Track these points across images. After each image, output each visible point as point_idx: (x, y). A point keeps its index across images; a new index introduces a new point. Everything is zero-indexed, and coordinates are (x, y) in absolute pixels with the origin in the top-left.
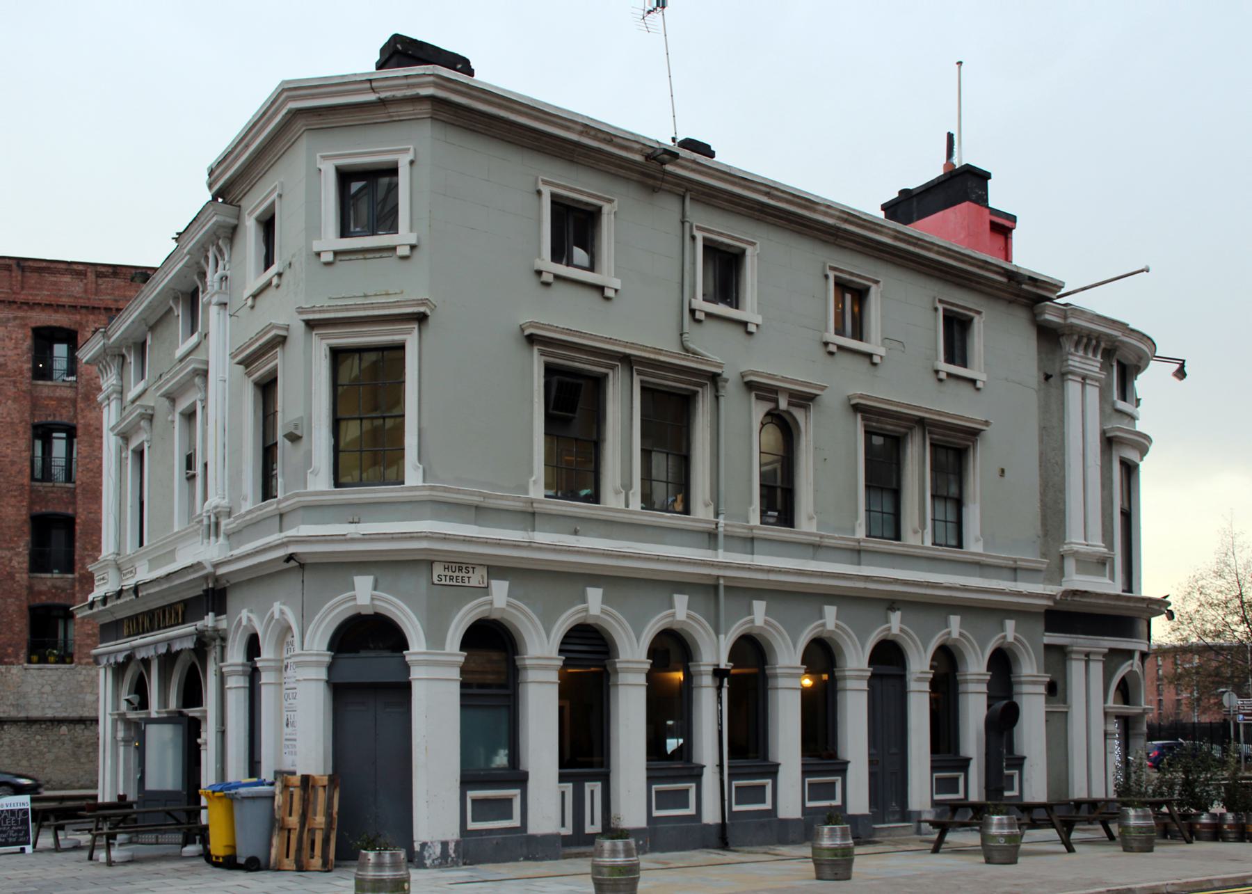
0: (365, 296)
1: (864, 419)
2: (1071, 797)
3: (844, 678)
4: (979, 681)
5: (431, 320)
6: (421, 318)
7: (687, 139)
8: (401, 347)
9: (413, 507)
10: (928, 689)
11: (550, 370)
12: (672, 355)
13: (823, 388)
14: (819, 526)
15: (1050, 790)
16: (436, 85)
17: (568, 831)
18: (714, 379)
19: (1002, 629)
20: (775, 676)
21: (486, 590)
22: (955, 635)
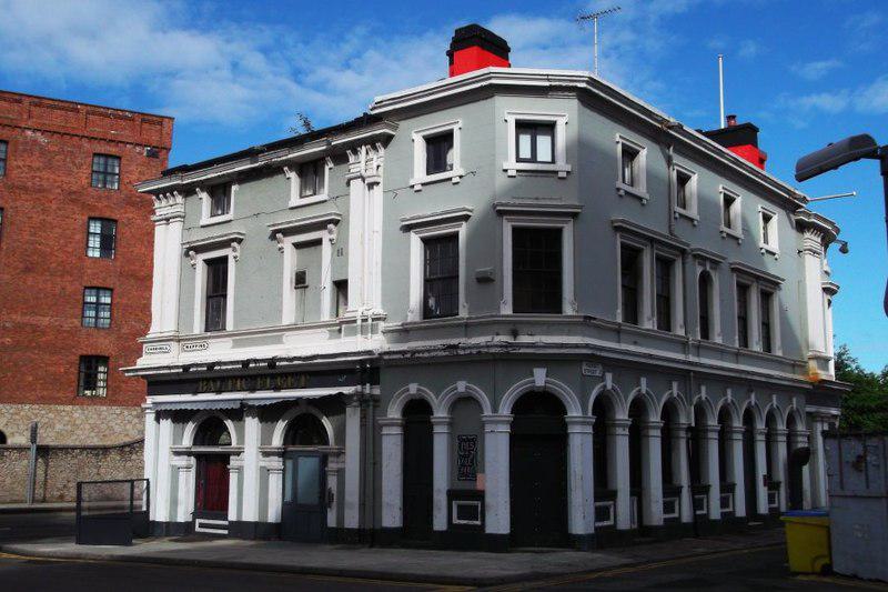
0: (537, 199)
1: (738, 276)
2: (346, 526)
3: (777, 434)
4: (715, 431)
5: (580, 216)
6: (574, 215)
7: (472, 26)
8: (560, 231)
9: (569, 326)
10: (591, 431)
11: (623, 246)
12: (664, 236)
13: (783, 280)
14: (784, 353)
15: (338, 523)
16: (587, 82)
17: (635, 526)
18: (683, 252)
19: (639, 384)
20: (648, 428)
21: (603, 378)
22: (644, 392)
